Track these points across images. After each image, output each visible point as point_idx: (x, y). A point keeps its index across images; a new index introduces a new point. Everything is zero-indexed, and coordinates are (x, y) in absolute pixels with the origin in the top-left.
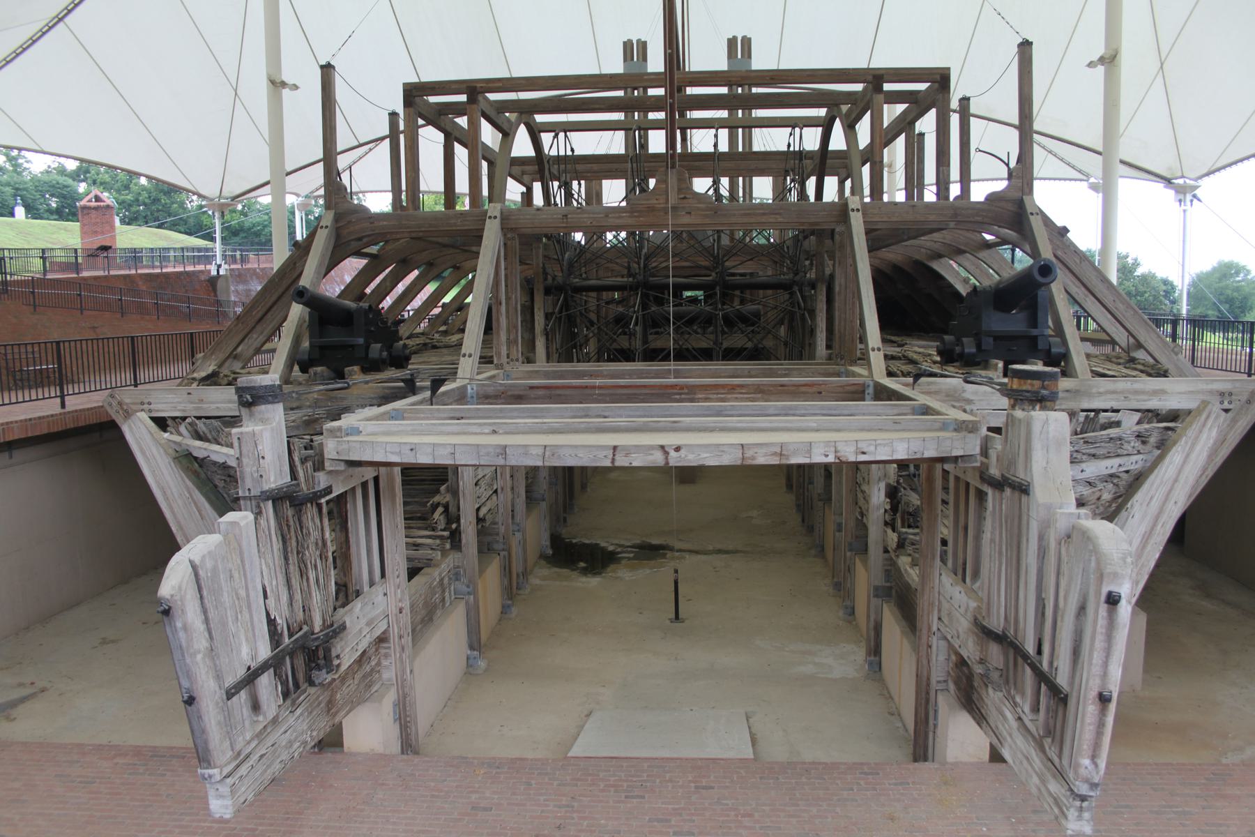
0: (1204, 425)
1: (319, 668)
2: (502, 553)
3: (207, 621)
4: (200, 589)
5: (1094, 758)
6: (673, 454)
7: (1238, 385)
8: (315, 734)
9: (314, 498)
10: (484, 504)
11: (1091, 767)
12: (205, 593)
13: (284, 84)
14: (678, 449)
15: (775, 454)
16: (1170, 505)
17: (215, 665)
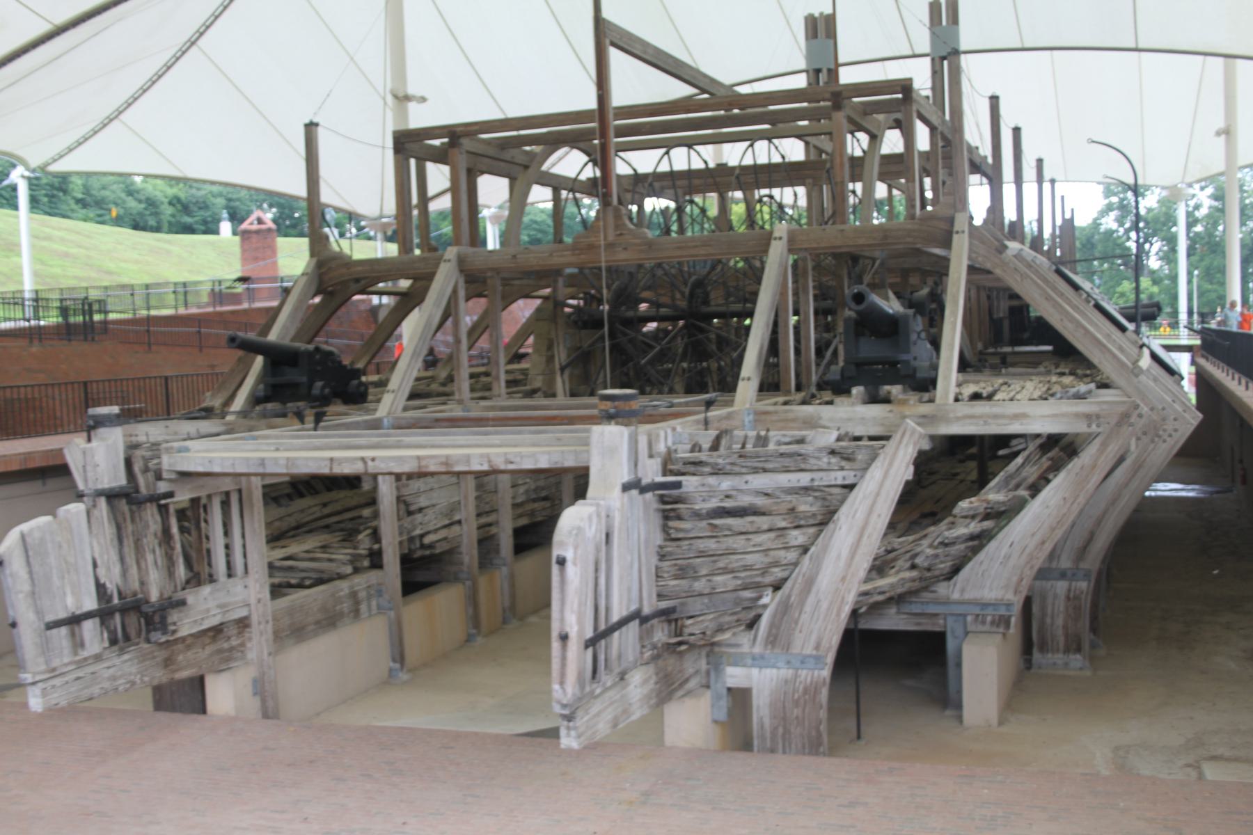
0: (900, 442)
1: (155, 630)
2: (468, 583)
3: (31, 573)
4: (26, 551)
5: (562, 683)
6: (370, 463)
7: (1105, 407)
8: (146, 679)
9: (154, 499)
10: (428, 533)
11: (560, 691)
12: (31, 553)
13: (407, 98)
14: (373, 460)
15: (442, 463)
16: (874, 518)
17: (36, 605)
